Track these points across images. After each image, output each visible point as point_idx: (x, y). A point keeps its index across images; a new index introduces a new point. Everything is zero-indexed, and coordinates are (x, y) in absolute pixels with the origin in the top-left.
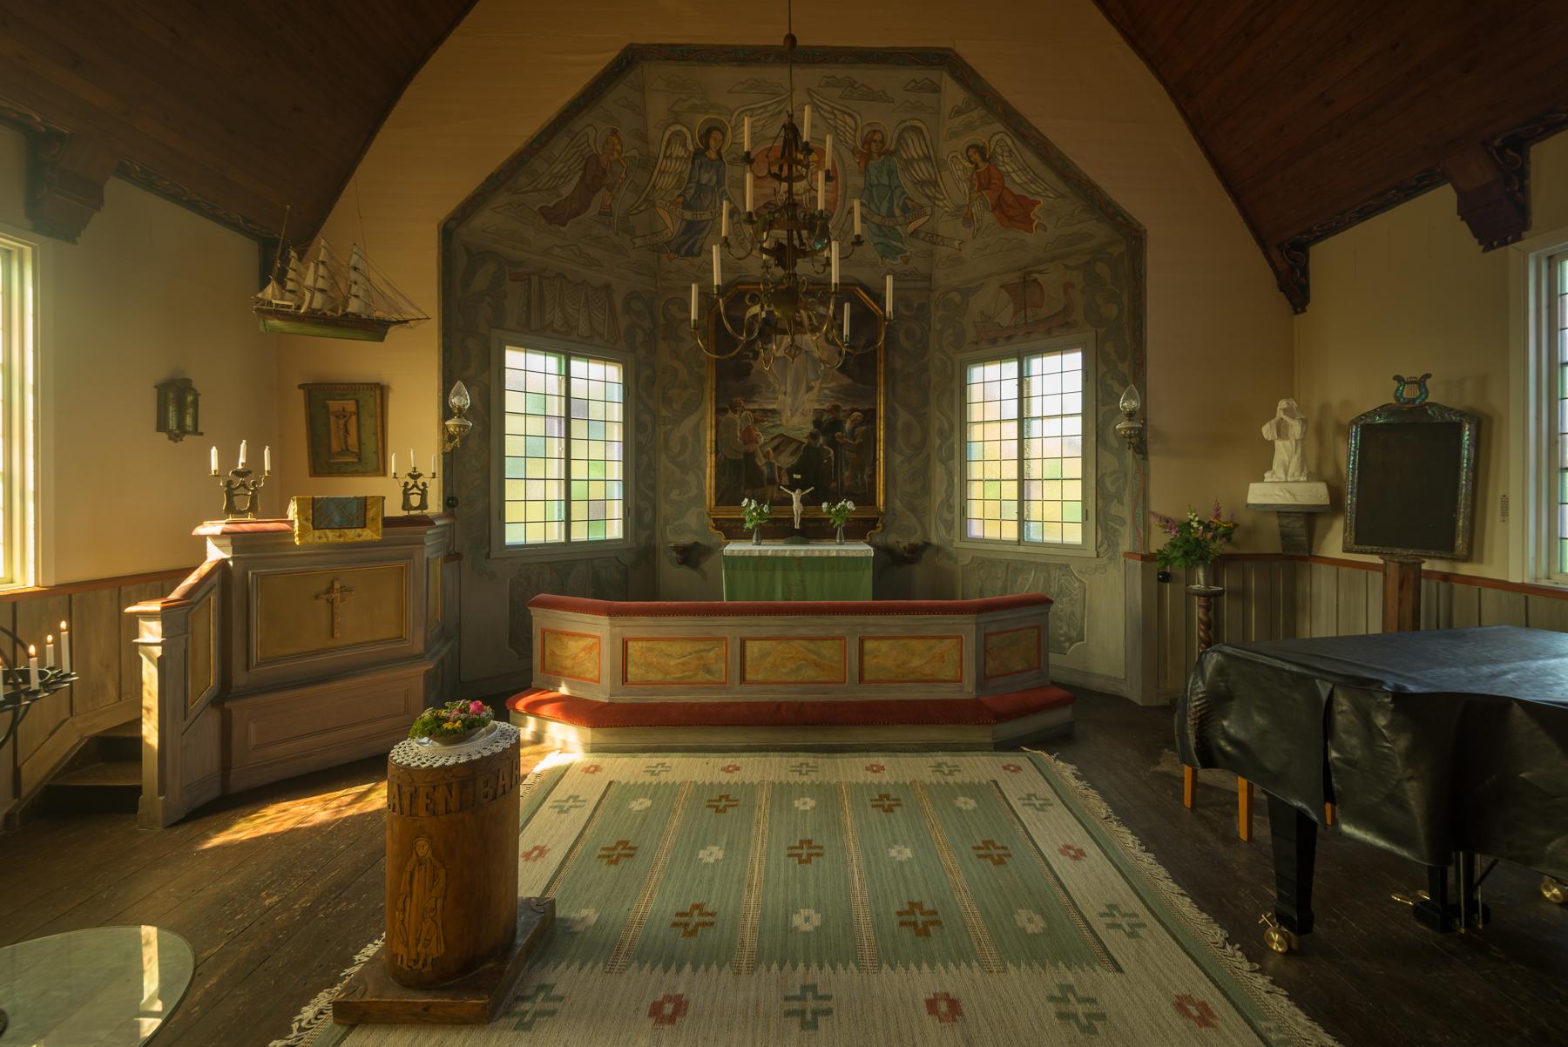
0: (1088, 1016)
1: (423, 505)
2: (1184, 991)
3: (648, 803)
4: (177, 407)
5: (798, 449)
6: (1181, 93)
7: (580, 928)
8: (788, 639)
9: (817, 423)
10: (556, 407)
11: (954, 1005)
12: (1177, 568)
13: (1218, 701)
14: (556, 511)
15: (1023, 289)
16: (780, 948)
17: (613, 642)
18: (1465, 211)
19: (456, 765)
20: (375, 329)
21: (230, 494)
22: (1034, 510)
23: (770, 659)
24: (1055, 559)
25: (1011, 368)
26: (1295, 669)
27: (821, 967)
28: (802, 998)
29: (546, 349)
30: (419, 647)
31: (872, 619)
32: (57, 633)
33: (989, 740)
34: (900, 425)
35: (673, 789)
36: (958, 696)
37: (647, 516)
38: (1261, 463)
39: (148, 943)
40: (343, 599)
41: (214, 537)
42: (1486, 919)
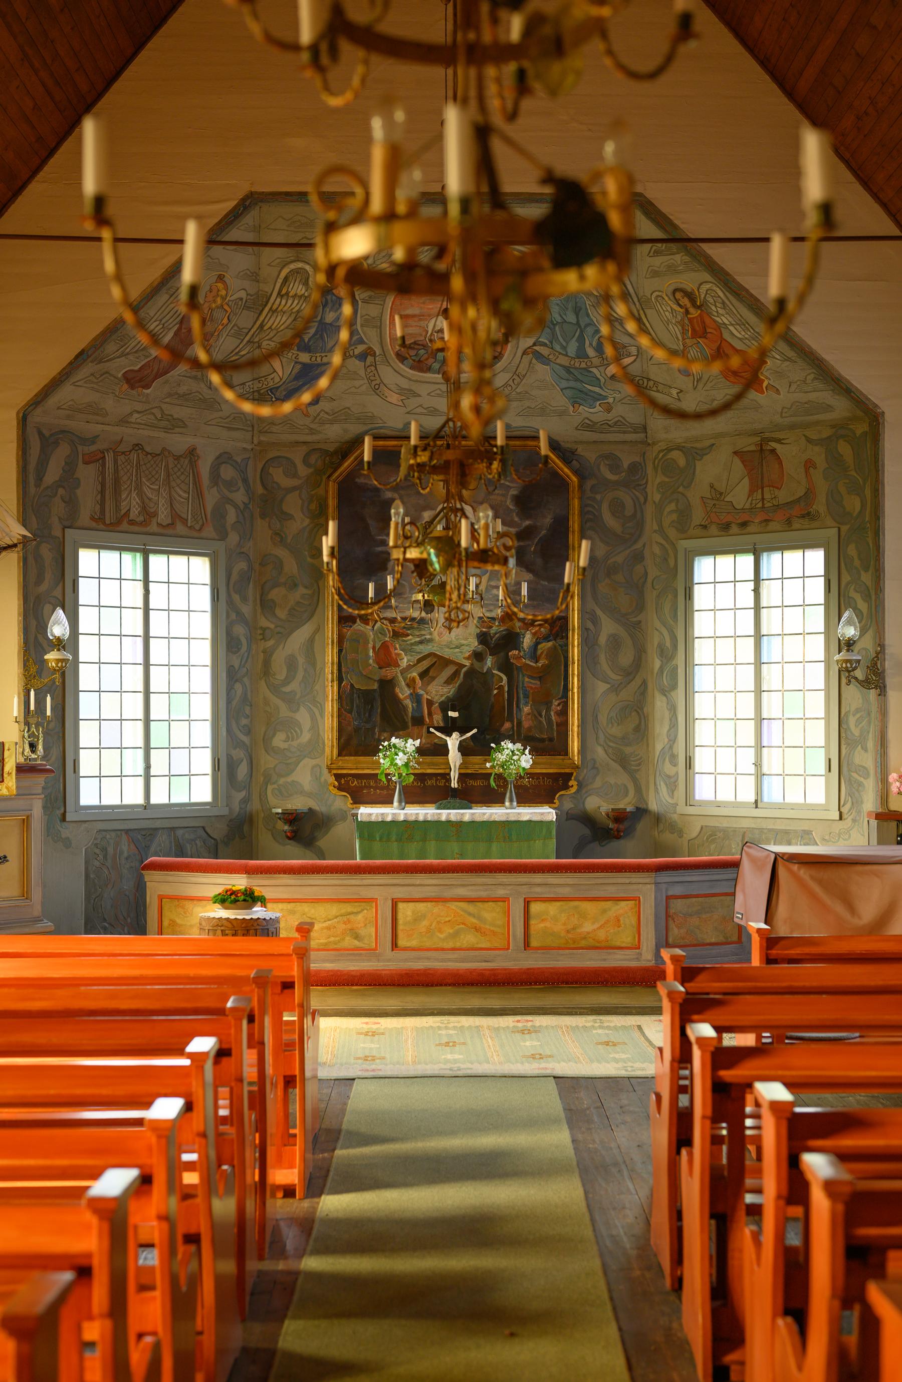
5: (456, 674)
9: (483, 638)
14: (134, 762)
15: (760, 458)
25: (746, 561)
31: (538, 878)
34: (603, 639)
36: (634, 964)
37: (242, 771)
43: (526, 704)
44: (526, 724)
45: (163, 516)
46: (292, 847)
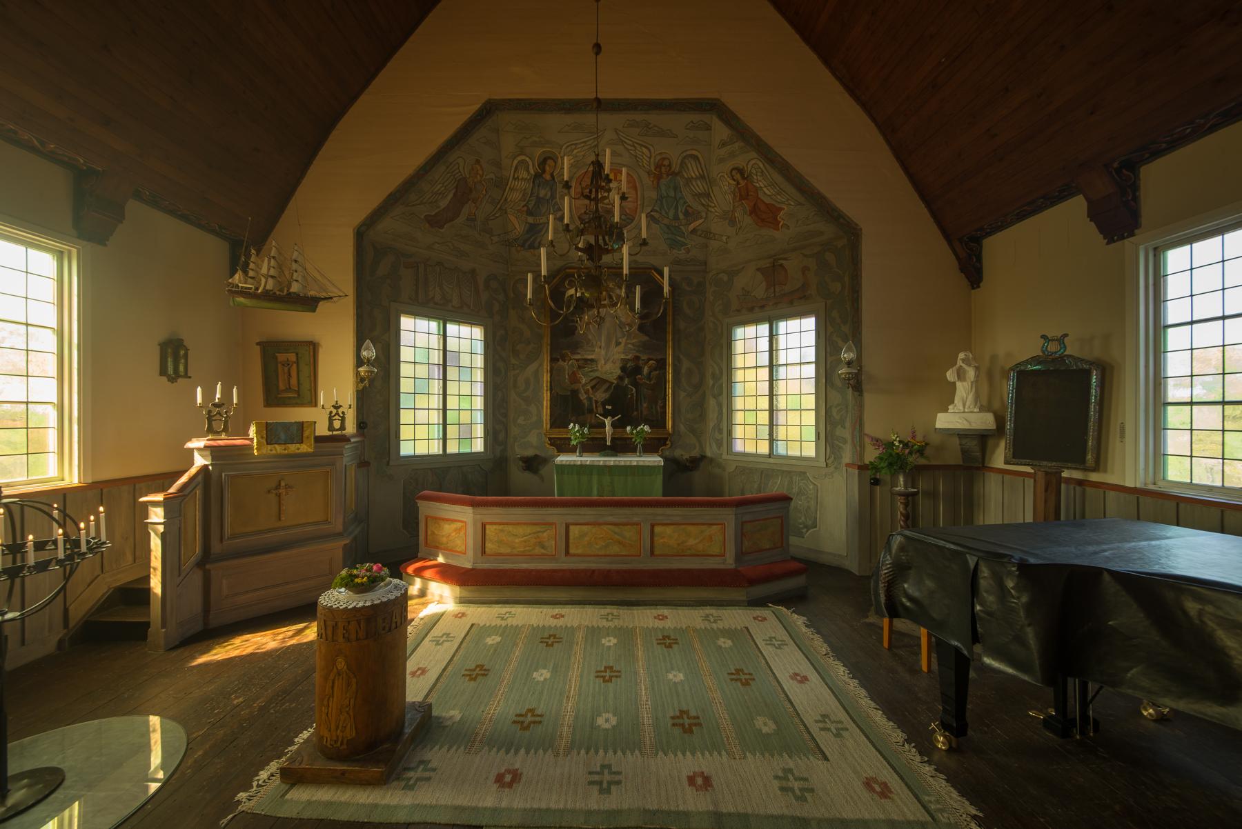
0: (801, 790)
1: (343, 428)
2: (872, 774)
3: (498, 639)
4: (173, 358)
6: (887, 129)
7: (449, 723)
9: (623, 369)
10: (436, 357)
11: (707, 781)
12: (884, 475)
13: (901, 570)
14: (436, 432)
15: (773, 271)
16: (587, 739)
17: (475, 525)
18: (1094, 215)
19: (364, 607)
20: (309, 303)
21: (210, 418)
22: (781, 432)
23: (587, 539)
24: (795, 468)
25: (764, 329)
26: (952, 547)
27: (615, 753)
28: (600, 773)
29: (429, 316)
30: (338, 526)
31: (659, 510)
32: (97, 514)
33: (744, 598)
34: (683, 371)
35: (516, 630)
36: (722, 567)
37: (501, 436)
38: (946, 397)
39: (154, 731)
40: (287, 493)
41: (199, 449)
42: (1096, 730)
44: (645, 412)
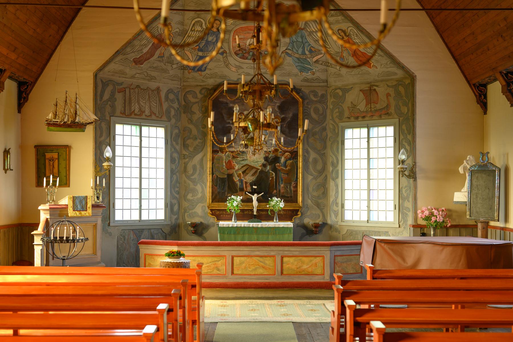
5: (256, 172)
8: (252, 256)
9: (266, 159)
14: (136, 204)
15: (370, 92)
25: (364, 131)
31: (286, 248)
34: (311, 160)
36: (322, 281)
37: (176, 208)
43: (282, 183)
44: (282, 191)
45: (147, 112)
46: (194, 236)
